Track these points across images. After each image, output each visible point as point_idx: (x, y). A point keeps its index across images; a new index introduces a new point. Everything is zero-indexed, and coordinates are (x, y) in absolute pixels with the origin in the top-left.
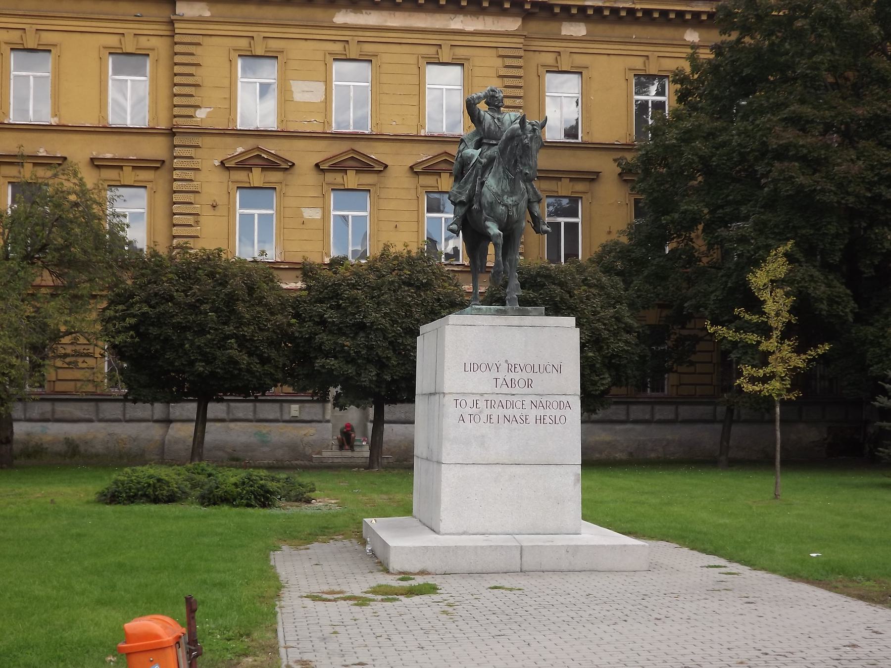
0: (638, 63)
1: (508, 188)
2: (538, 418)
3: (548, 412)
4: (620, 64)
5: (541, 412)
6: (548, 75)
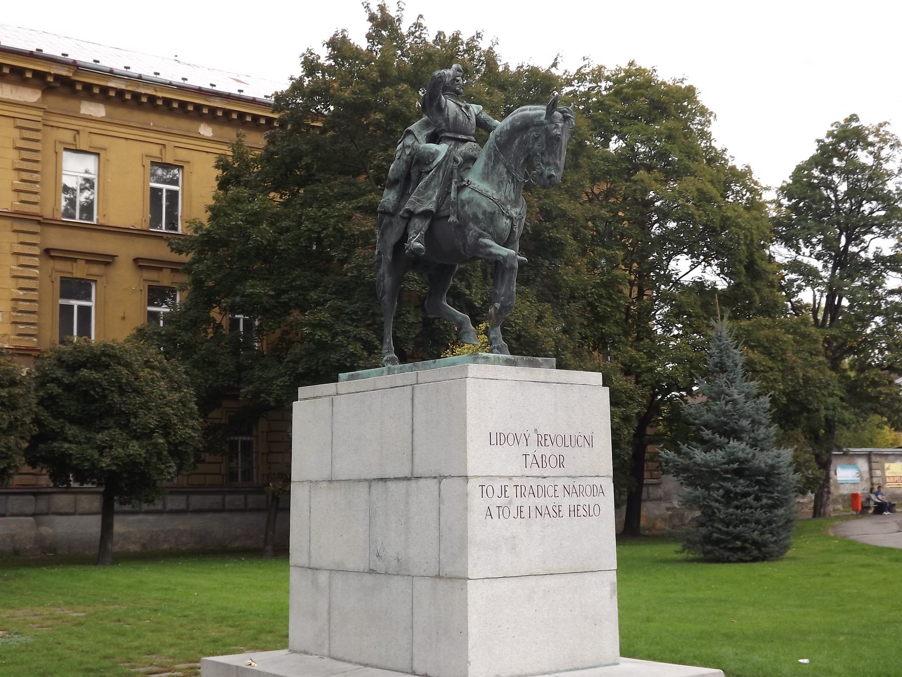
0: (155, 151)
1: (513, 195)
2: (572, 509)
5: (574, 500)
6: (66, 154)
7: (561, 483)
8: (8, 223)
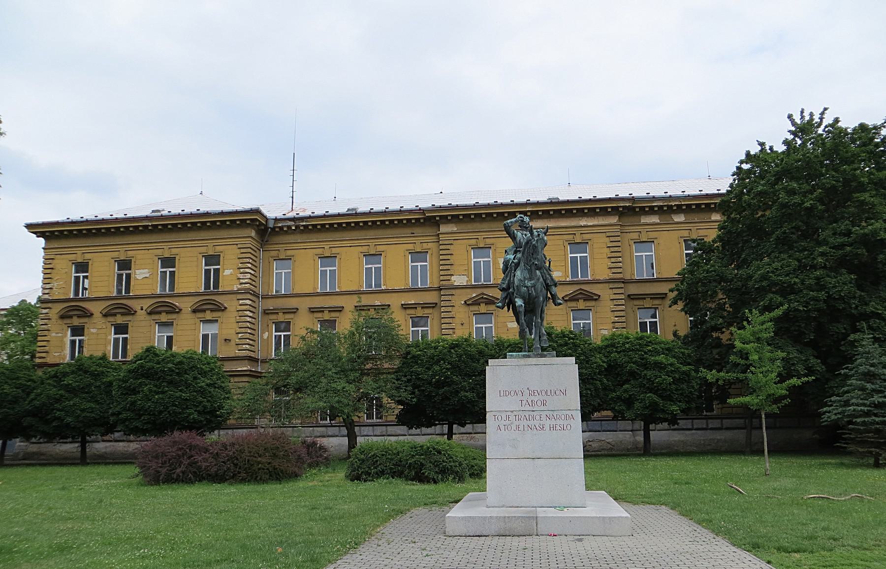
0: (686, 234)
3: (558, 422)
4: (675, 235)
5: (553, 422)
7: (544, 414)
8: (607, 285)
